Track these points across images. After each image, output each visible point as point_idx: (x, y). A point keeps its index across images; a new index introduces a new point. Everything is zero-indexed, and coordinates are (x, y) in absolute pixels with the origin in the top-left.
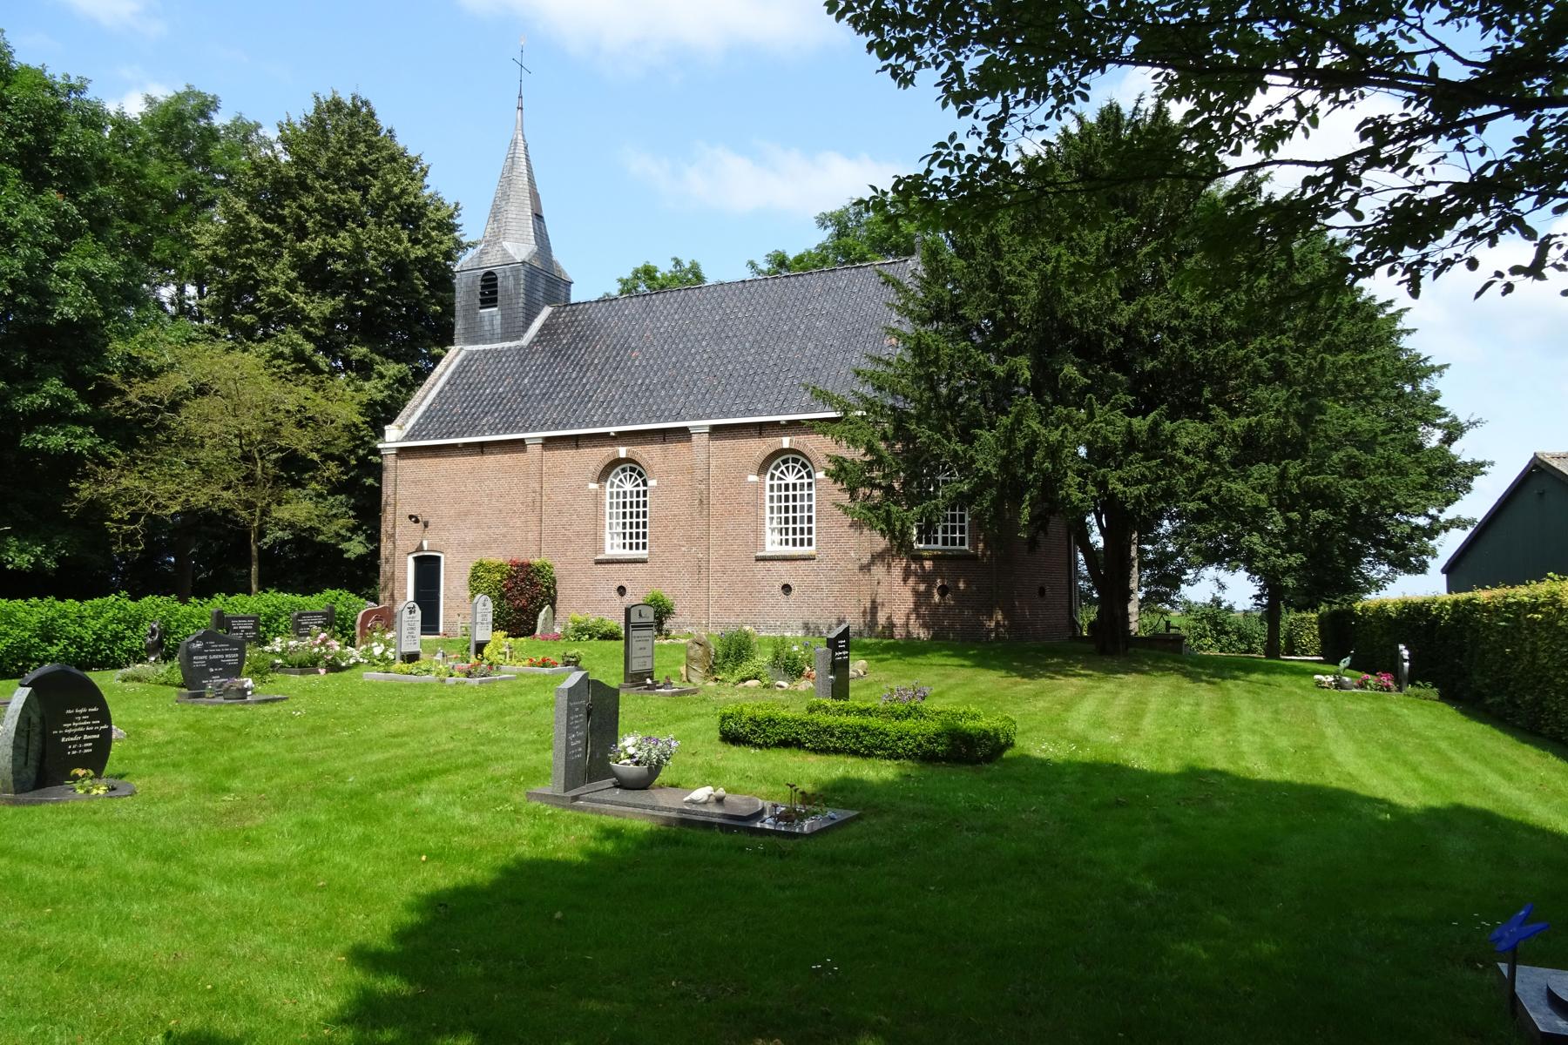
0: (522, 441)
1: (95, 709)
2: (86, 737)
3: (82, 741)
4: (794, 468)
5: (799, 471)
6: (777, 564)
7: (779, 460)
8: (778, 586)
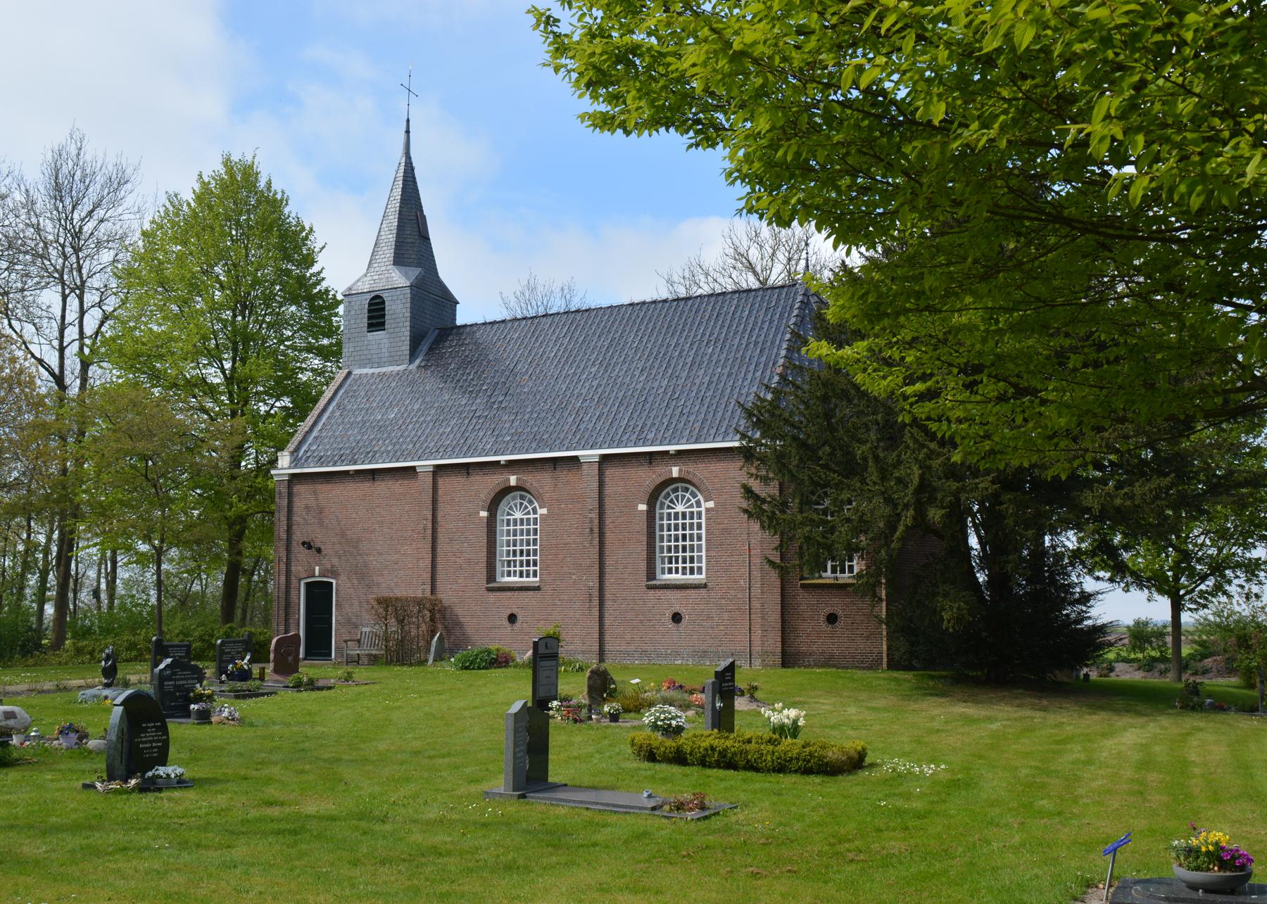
0: (413, 468)
3: (152, 748)
4: (672, 501)
5: (683, 496)
6: (668, 593)
7: (668, 489)
8: (668, 614)
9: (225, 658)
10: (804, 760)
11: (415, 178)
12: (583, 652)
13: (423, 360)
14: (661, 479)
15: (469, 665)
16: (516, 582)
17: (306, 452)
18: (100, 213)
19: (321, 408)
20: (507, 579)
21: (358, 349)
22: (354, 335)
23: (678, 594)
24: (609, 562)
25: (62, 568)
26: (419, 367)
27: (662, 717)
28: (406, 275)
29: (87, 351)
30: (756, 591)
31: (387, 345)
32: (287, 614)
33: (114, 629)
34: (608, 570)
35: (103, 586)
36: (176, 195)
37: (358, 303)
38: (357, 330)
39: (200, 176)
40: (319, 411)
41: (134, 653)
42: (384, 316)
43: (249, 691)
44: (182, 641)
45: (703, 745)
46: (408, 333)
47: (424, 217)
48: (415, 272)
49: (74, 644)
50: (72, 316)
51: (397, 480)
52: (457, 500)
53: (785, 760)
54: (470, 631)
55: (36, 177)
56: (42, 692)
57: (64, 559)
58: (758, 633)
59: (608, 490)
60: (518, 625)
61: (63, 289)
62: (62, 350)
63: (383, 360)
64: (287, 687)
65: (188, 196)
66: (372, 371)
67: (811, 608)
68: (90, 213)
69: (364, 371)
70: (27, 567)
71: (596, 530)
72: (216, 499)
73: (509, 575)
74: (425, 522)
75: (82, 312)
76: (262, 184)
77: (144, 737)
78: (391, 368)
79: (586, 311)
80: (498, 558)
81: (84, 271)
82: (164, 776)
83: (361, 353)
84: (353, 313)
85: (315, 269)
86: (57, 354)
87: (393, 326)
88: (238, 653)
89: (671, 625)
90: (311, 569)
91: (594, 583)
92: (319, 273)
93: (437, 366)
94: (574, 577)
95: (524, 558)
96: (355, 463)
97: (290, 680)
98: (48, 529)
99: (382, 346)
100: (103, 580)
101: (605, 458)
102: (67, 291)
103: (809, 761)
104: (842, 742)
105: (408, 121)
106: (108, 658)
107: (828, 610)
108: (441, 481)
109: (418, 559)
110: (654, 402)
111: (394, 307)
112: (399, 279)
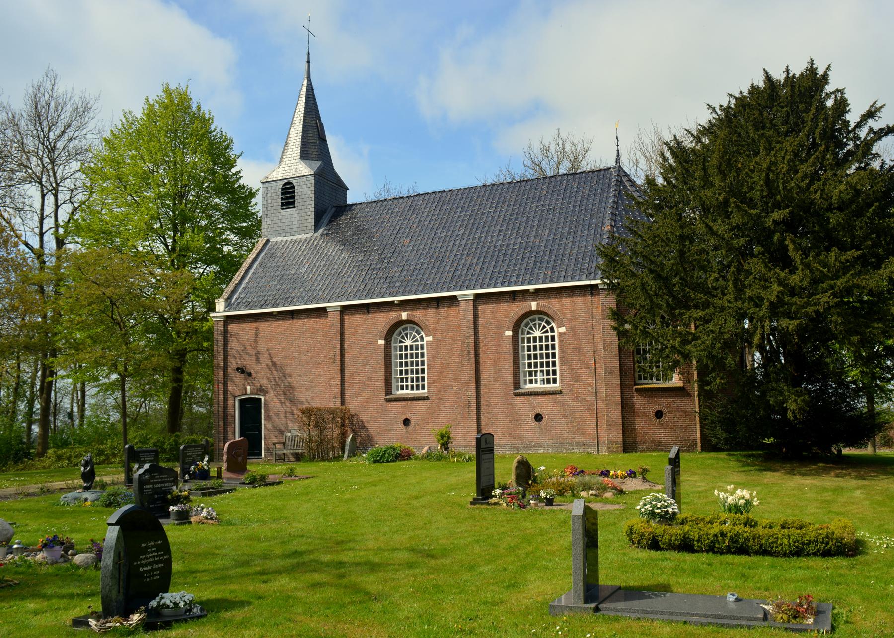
0: (324, 308)
1: (160, 542)
2: (155, 566)
3: (153, 570)
5: (544, 327)
6: (531, 398)
7: (528, 320)
8: (532, 415)
9: (188, 460)
10: (823, 543)
11: (314, 96)
12: (465, 446)
13: (325, 230)
14: (523, 312)
15: (380, 459)
16: (409, 394)
17: (237, 299)
18: (70, 133)
19: (247, 266)
20: (400, 392)
21: (274, 222)
22: (270, 212)
23: (539, 399)
24: (483, 376)
25: (44, 396)
26: (322, 235)
27: (659, 505)
28: (310, 166)
29: (61, 231)
30: (602, 394)
31: (296, 219)
32: (225, 424)
33: (85, 440)
34: (482, 382)
35: (75, 409)
36: (130, 112)
37: (273, 188)
38: (273, 208)
39: (147, 100)
40: (246, 268)
41: (103, 458)
42: (293, 197)
43: (213, 488)
44: (140, 448)
45: (712, 532)
46: (313, 210)
47: (322, 125)
48: (318, 164)
49: (55, 452)
50: (49, 209)
51: (311, 318)
52: (360, 332)
53: (803, 544)
54: (373, 432)
55: (20, 105)
56: (29, 495)
57: (47, 388)
58: (604, 427)
59: (481, 321)
60: (411, 427)
61: (42, 191)
62: (42, 235)
63: (294, 230)
64: (244, 483)
65: (138, 113)
66: (285, 238)
67: (643, 406)
68: (63, 133)
69: (280, 239)
70: (17, 393)
71: (473, 352)
72: (164, 338)
73: (402, 389)
74: (334, 350)
75: (57, 207)
76: (194, 108)
77: (144, 559)
78: (300, 236)
79: (450, 191)
80: (393, 376)
81: (59, 175)
82: (172, 605)
83: (277, 225)
84: (269, 195)
85: (234, 170)
86: (38, 238)
87: (301, 204)
88: (198, 455)
89: (534, 424)
90: (241, 388)
91: (472, 393)
92: (239, 172)
93: (337, 233)
94: (455, 389)
95: (415, 375)
96: (277, 306)
97: (243, 478)
98: (33, 368)
99: (293, 220)
100: (75, 405)
101: (477, 296)
102: (45, 192)
103: (827, 543)
104: (837, 526)
105: (309, 53)
106: (87, 464)
107: (656, 408)
108: (346, 318)
109: (330, 379)
110: (511, 255)
111: (301, 190)
112: (305, 169)
